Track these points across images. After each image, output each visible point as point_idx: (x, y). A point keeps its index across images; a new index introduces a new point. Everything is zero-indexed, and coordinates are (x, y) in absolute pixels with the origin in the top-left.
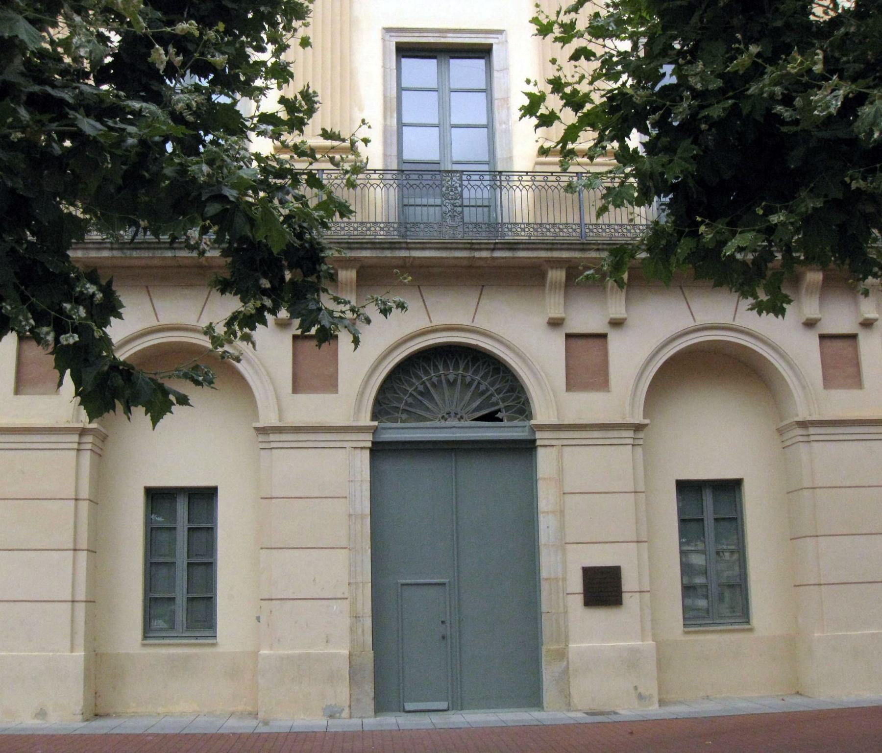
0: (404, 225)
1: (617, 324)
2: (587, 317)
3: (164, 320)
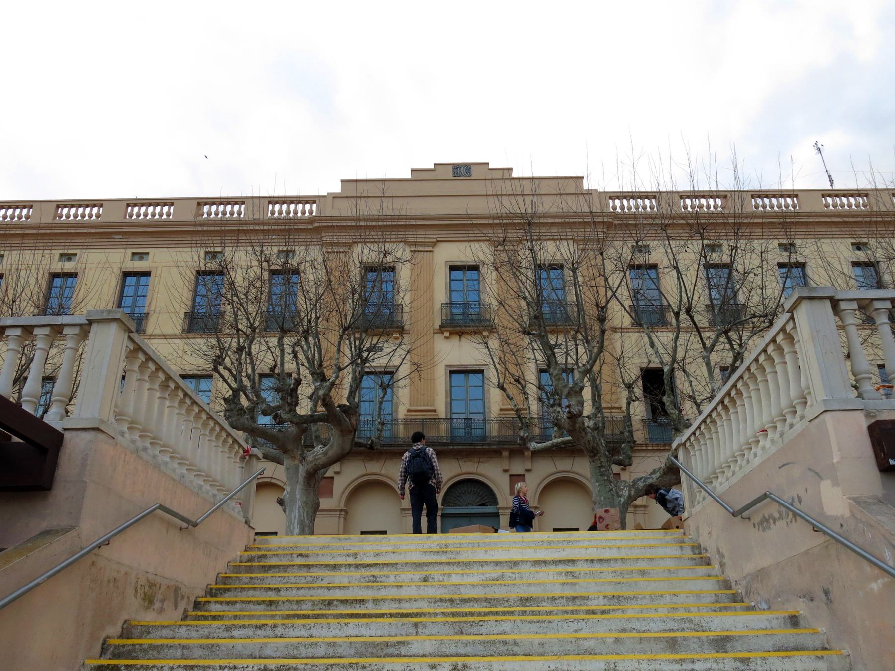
0: (453, 438)
1: (528, 471)
2: (518, 467)
3: (369, 471)
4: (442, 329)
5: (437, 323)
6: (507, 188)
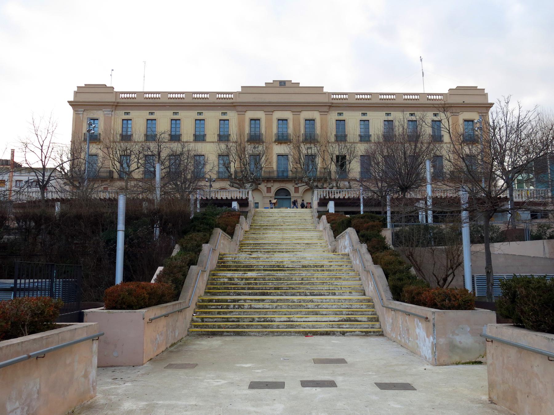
4: (275, 142)
5: (274, 140)
6: (297, 90)
